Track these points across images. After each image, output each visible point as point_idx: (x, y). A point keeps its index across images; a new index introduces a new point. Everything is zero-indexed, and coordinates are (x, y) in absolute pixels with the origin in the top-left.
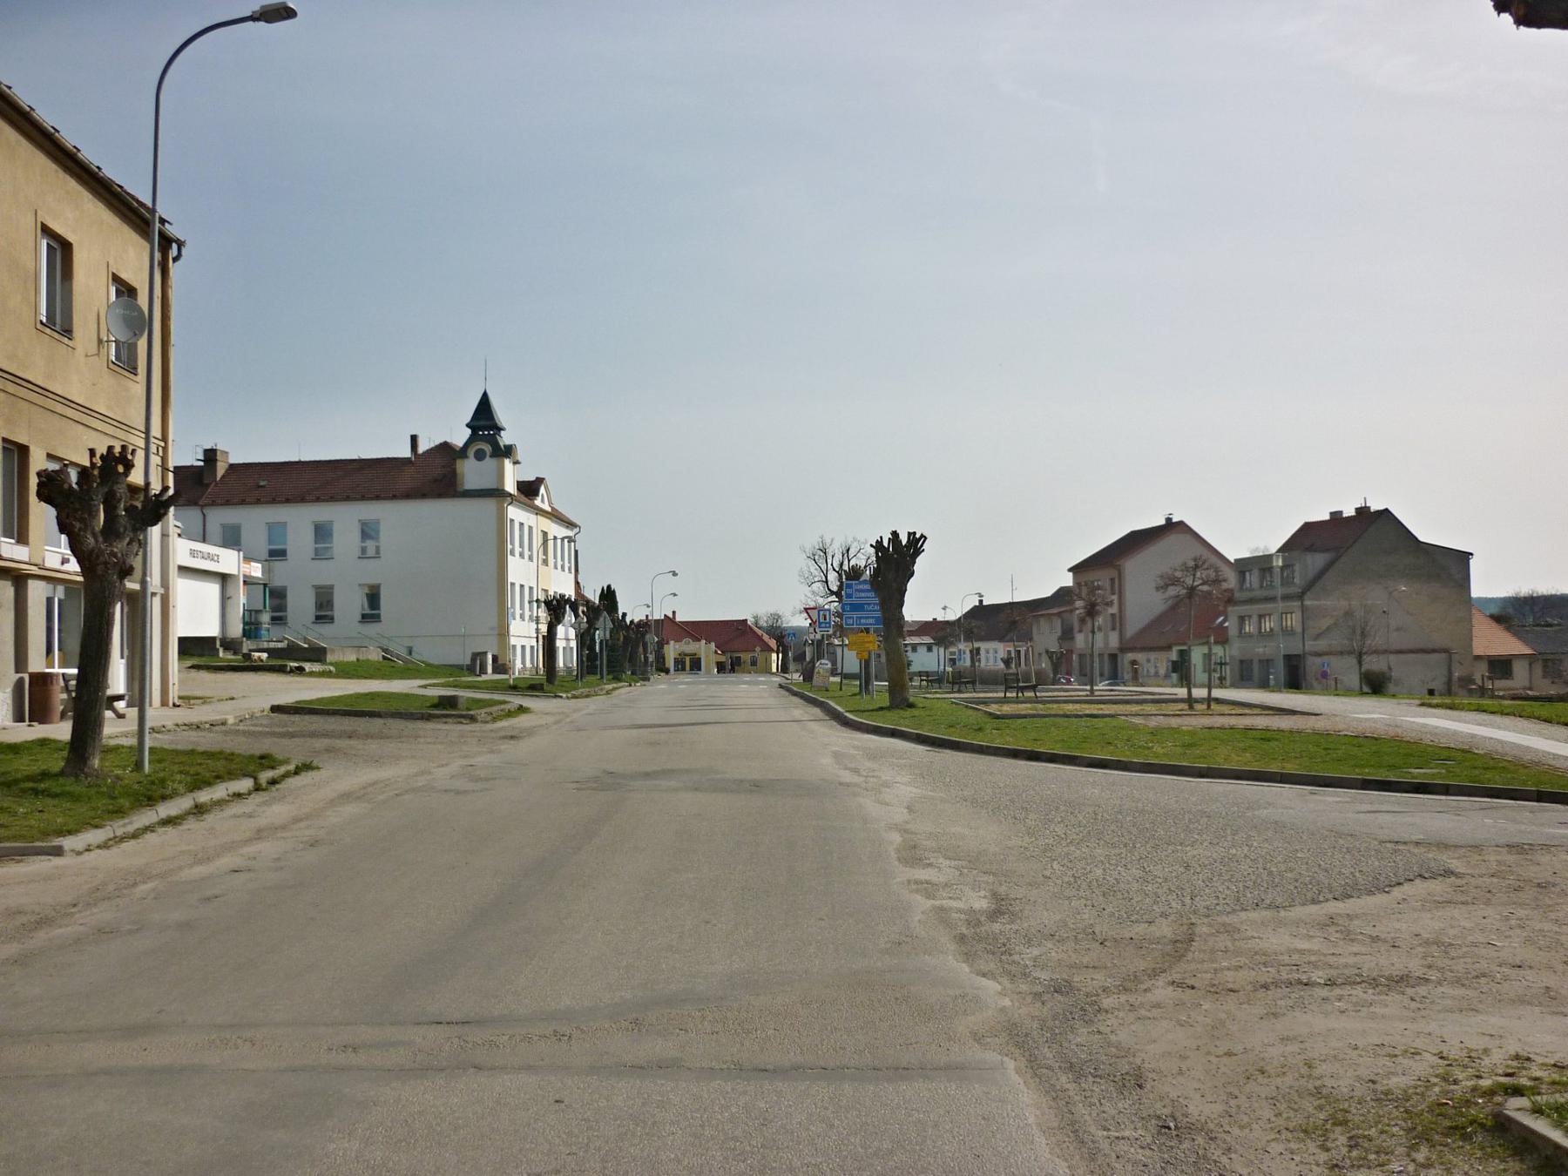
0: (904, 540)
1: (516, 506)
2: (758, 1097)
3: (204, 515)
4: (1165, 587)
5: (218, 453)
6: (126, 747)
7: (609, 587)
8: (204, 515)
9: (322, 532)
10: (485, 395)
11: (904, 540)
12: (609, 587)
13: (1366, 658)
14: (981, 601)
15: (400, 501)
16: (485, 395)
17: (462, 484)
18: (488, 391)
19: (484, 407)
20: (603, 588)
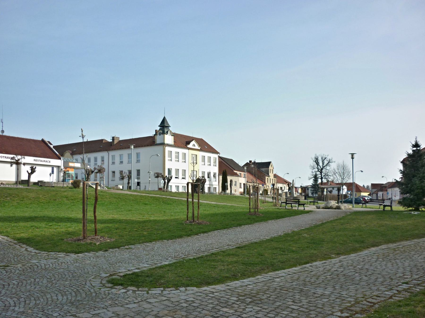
0: (314, 181)
1: (167, 146)
2: (267, 233)
3: (109, 153)
4: (340, 260)
5: (115, 138)
6: (26, 239)
7: (225, 170)
8: (109, 153)
9: (121, 156)
10: (164, 118)
11: (314, 181)
12: (225, 170)
13: (204, 164)
14: (87, 140)
15: (144, 147)
16: (164, 118)
17: (156, 142)
18: (167, 118)
19: (164, 120)
20: (224, 170)
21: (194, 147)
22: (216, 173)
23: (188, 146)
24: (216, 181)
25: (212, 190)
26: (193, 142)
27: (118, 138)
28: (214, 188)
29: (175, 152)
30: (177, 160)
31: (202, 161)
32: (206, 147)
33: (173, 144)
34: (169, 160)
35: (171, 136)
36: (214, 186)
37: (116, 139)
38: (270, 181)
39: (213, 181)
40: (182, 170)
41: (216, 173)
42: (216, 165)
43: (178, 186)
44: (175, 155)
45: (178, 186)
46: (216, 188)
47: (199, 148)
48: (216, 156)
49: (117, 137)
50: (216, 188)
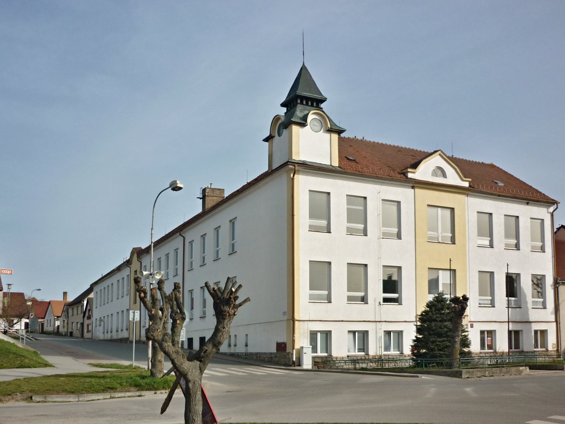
10: (303, 69)
13: (487, 243)
16: (303, 69)
21: (440, 180)
22: (544, 276)
23: (410, 175)
24: (330, 302)
25: (527, 344)
26: (436, 161)
27: (218, 192)
28: (536, 332)
29: (345, 199)
30: (324, 223)
31: (480, 234)
32: (501, 184)
33: (336, 163)
34: (313, 229)
35: (327, 135)
36: (535, 327)
37: (210, 194)
38: (120, 397)
39: (530, 305)
40: (310, 261)
41: (544, 276)
42: (543, 249)
43: (365, 334)
44: (347, 209)
45: (365, 334)
46: (544, 333)
47: (466, 184)
48: (542, 212)
49: (213, 190)
50: (544, 333)
